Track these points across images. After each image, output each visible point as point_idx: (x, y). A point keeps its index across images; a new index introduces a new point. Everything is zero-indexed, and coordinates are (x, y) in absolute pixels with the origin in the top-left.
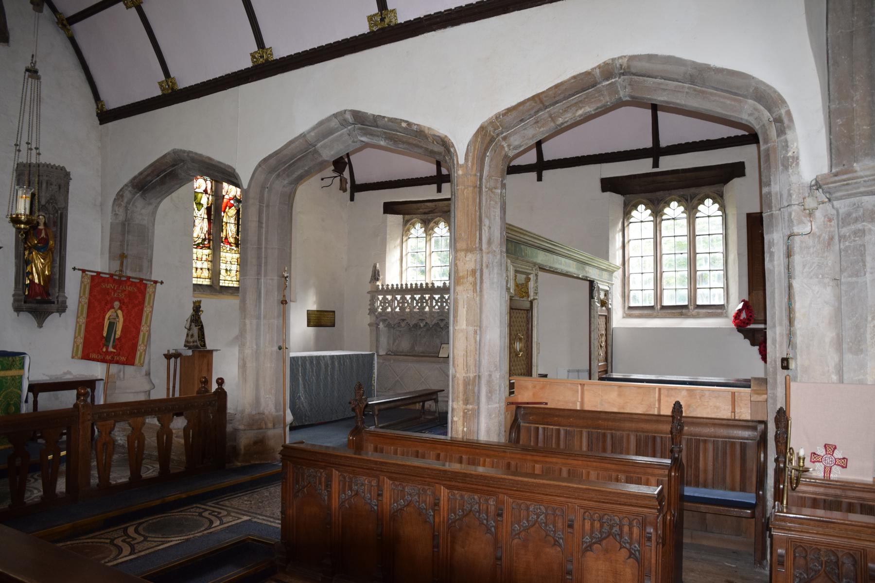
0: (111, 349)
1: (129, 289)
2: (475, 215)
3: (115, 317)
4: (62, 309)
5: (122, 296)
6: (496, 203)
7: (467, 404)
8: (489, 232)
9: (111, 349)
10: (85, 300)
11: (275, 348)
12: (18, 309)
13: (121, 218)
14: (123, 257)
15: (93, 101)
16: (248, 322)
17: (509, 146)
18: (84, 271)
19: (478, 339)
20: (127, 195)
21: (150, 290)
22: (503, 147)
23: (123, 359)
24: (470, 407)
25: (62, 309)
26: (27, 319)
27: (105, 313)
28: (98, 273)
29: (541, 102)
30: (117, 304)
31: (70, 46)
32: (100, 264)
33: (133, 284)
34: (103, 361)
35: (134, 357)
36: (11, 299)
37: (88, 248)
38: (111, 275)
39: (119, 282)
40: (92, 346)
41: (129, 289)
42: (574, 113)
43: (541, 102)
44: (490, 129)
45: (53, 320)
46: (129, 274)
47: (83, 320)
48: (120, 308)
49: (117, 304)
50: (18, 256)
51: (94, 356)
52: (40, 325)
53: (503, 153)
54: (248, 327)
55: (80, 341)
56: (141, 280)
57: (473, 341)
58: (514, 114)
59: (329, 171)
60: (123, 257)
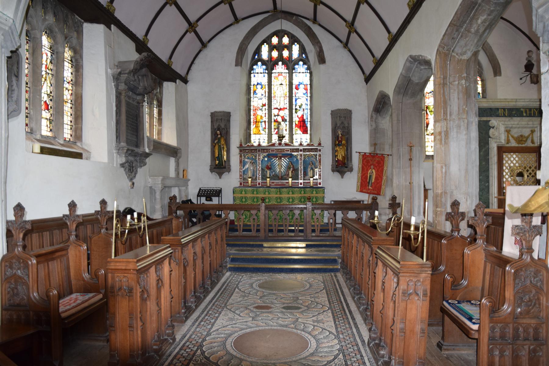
0: (370, 188)
1: (377, 159)
2: (441, 100)
3: (372, 173)
4: (351, 170)
5: (375, 163)
6: (455, 90)
7: (437, 208)
8: (450, 109)
9: (370, 188)
10: (360, 166)
11: (408, 183)
12: (333, 171)
13: (374, 126)
14: (375, 145)
15: (362, 75)
16: (394, 170)
17: (457, 54)
18: (360, 153)
19: (444, 170)
20: (374, 116)
21: (386, 159)
22: (454, 56)
23: (376, 192)
24: (439, 209)
25: (351, 170)
26: (337, 174)
27: (368, 171)
28: (365, 153)
29: (455, 25)
30: (372, 167)
31: (350, 54)
32: (366, 149)
33: (379, 157)
34: (367, 193)
35: (380, 192)
36: (331, 167)
37: (361, 143)
38: (370, 154)
39: (373, 157)
40: (363, 186)
41: (377, 159)
42: (477, 23)
43: (455, 25)
44: (441, 49)
45: (348, 174)
46: (378, 152)
47: (360, 175)
48: (374, 169)
49: (372, 167)
50: (333, 149)
51: (364, 191)
52: (342, 177)
53: (456, 59)
54: (394, 173)
55: (359, 184)
56: (382, 155)
57: (440, 172)
58: (446, 36)
59: (92, 159)
60: (375, 145)
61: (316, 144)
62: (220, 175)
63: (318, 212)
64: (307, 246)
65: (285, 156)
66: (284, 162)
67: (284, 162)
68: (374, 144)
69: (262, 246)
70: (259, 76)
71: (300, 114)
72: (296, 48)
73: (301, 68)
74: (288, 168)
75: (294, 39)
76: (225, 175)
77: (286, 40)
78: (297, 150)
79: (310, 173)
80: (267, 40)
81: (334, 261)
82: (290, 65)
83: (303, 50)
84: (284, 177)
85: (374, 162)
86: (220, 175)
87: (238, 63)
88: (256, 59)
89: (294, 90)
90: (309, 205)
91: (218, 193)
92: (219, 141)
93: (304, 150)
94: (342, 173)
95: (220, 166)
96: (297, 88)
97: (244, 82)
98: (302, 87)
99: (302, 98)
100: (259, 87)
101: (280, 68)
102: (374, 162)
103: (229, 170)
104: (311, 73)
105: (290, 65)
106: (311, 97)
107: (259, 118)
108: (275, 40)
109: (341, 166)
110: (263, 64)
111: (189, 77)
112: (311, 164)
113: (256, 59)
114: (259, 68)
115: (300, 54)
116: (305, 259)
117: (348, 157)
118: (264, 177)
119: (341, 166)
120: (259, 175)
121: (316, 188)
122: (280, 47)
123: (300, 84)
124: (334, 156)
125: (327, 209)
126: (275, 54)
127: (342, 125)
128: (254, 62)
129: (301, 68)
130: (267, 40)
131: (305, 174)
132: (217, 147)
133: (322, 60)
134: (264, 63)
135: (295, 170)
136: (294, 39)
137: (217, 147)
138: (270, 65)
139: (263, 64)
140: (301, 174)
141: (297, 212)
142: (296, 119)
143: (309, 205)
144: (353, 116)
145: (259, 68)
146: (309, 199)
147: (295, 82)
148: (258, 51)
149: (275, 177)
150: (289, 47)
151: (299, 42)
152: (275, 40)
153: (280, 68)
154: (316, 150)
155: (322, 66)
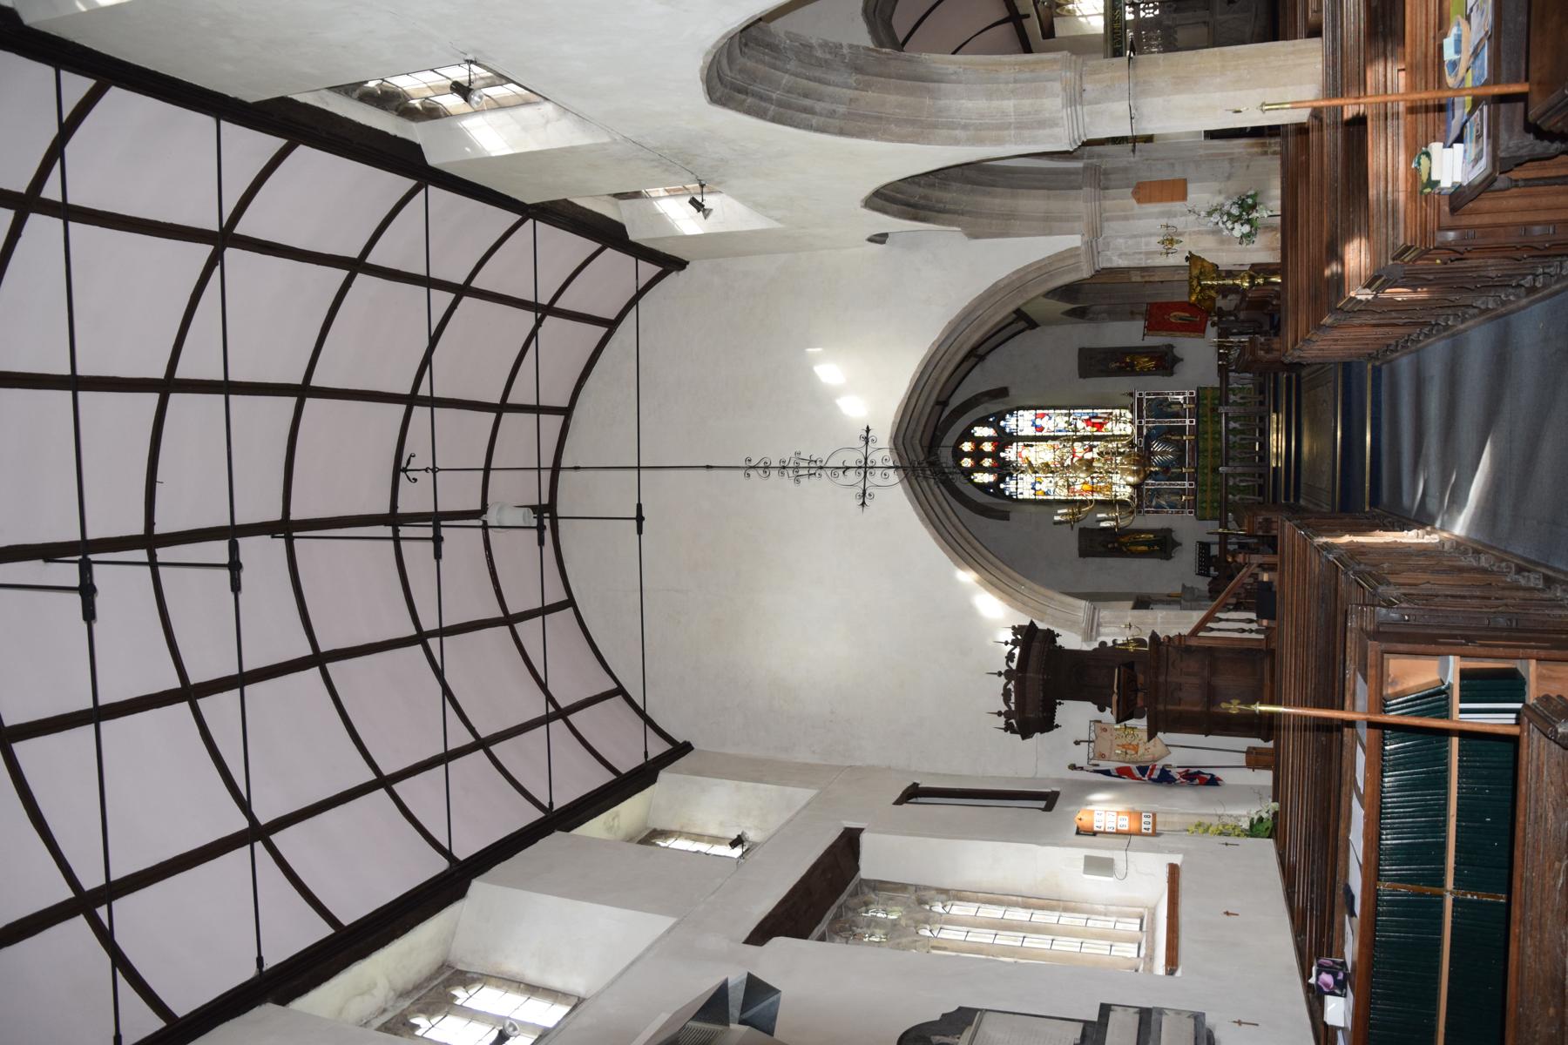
4: (1171, 347)
12: (1172, 374)
13: (1144, 362)
14: (1132, 313)
25: (1171, 347)
26: (1178, 367)
32: (1139, 325)
37: (1129, 333)
40: (1199, 330)
45: (1178, 352)
60: (1132, 313)
61: (1128, 400)
62: (1176, 544)
63: (1232, 398)
64: (1276, 411)
65: (1148, 445)
66: (1157, 447)
67: (1157, 447)
68: (1132, 315)
69: (1276, 469)
70: (1022, 487)
71: (1080, 425)
72: (980, 432)
73: (1010, 423)
74: (1166, 442)
75: (967, 435)
76: (1177, 537)
77: (967, 447)
78: (1140, 429)
79: (1176, 408)
80: (968, 473)
81: (1289, 379)
82: (1005, 439)
83: (983, 422)
84: (1180, 447)
85: (1158, 317)
86: (1176, 544)
87: (1004, 516)
88: (994, 490)
89: (1044, 433)
90: (1222, 410)
91: (1204, 547)
92: (1125, 544)
93: (1140, 417)
94: (1177, 360)
95: (1163, 545)
96: (1041, 429)
97: (1032, 508)
98: (1038, 422)
99: (1055, 422)
100: (1038, 487)
101: (1010, 454)
102: (1158, 317)
103: (1169, 531)
104: (1018, 409)
105: (1005, 439)
106: (1055, 408)
107: (1086, 487)
108: (967, 463)
109: (1165, 362)
110: (1004, 481)
111: (500, 1019)
112: (1161, 408)
113: (994, 490)
114: (1010, 486)
115: (989, 425)
116: (1344, 404)
117: (1149, 352)
118: (1181, 477)
119: (1165, 362)
120: (1177, 485)
121: (1197, 401)
122: (978, 455)
123: (1034, 424)
124: (1148, 372)
125: (1227, 383)
126: (987, 462)
127: (1097, 363)
128: (1000, 493)
129: (1010, 423)
130: (968, 473)
131: (1177, 415)
132: (1133, 548)
133: (1002, 393)
134: (1001, 479)
135: (1171, 430)
136: (967, 435)
137: (1133, 548)
138: (1005, 470)
139: (1004, 481)
140: (1176, 422)
141: (1232, 425)
142: (1089, 430)
143: (1222, 410)
144: (1087, 345)
145: (1010, 486)
146: (1214, 410)
147: (1030, 431)
148: (983, 487)
149: (1180, 461)
150: (979, 441)
151: (971, 426)
152: (967, 463)
153: (1010, 454)
154: (1140, 401)
155: (1012, 392)
